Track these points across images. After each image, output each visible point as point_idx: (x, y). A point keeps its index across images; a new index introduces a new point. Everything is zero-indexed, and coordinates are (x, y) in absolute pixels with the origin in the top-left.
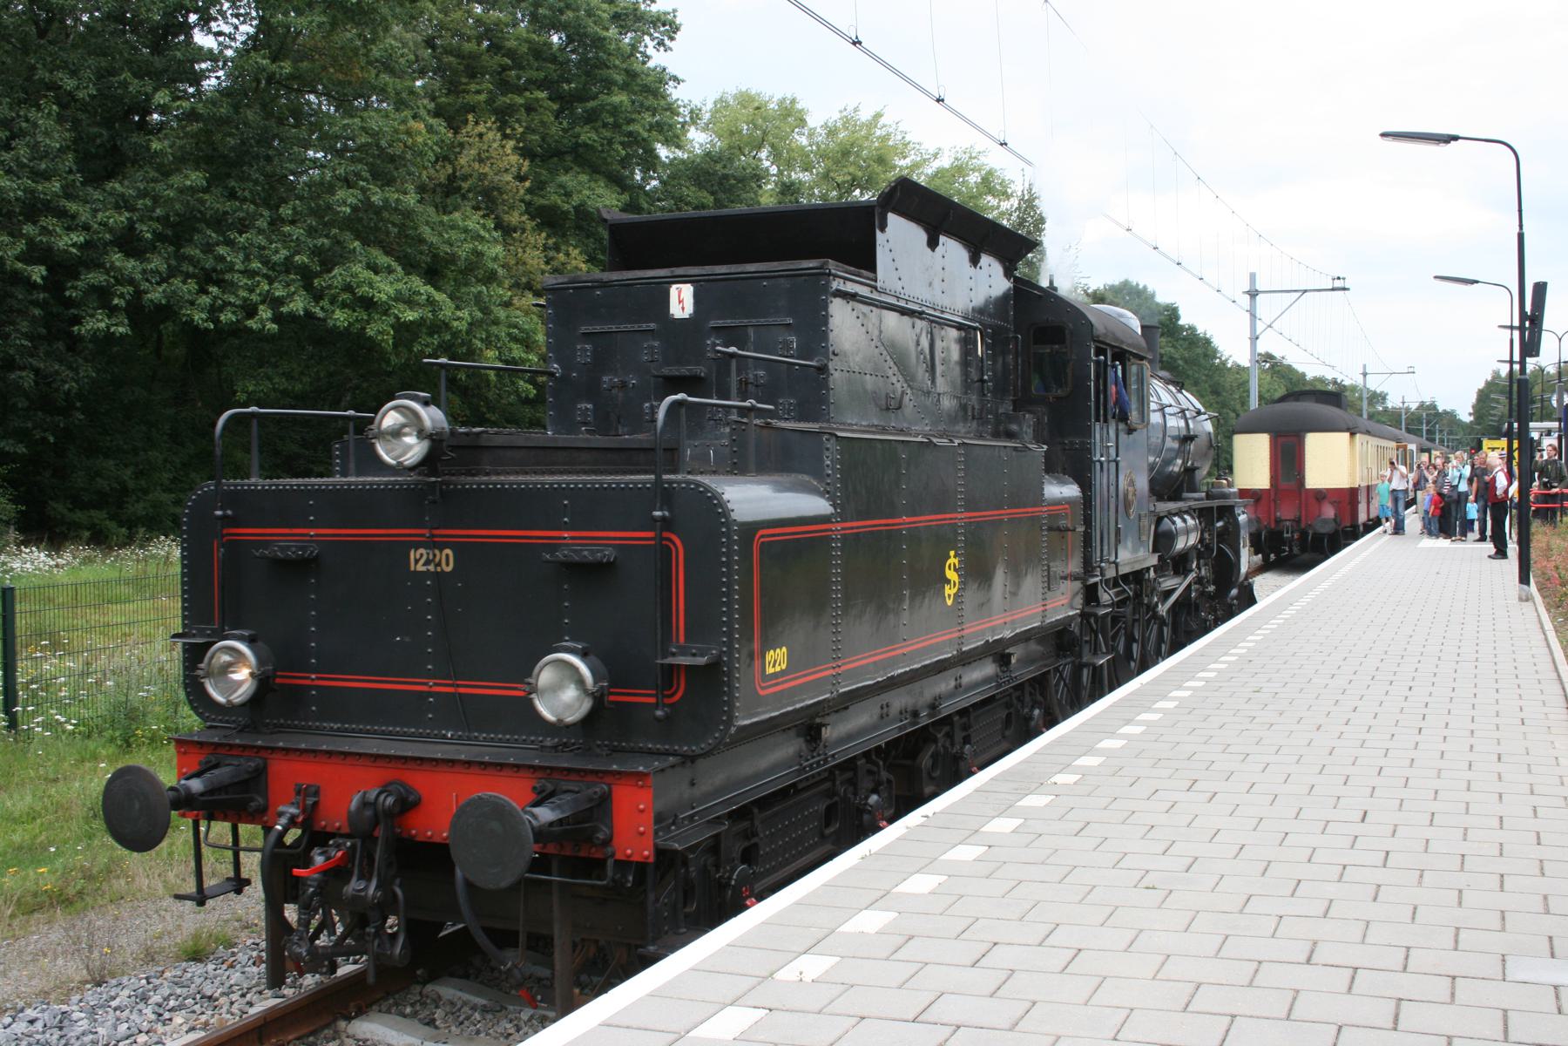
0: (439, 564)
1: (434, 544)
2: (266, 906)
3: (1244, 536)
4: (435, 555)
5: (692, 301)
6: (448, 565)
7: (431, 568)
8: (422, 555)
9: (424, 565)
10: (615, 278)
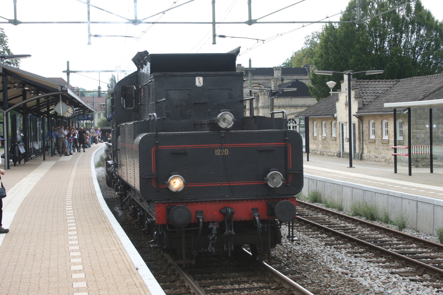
0: (224, 153)
1: (221, 148)
2: (281, 234)
3: (108, 143)
4: (223, 151)
5: (202, 82)
6: (227, 153)
7: (222, 154)
8: (219, 151)
9: (220, 153)
10: (178, 74)
